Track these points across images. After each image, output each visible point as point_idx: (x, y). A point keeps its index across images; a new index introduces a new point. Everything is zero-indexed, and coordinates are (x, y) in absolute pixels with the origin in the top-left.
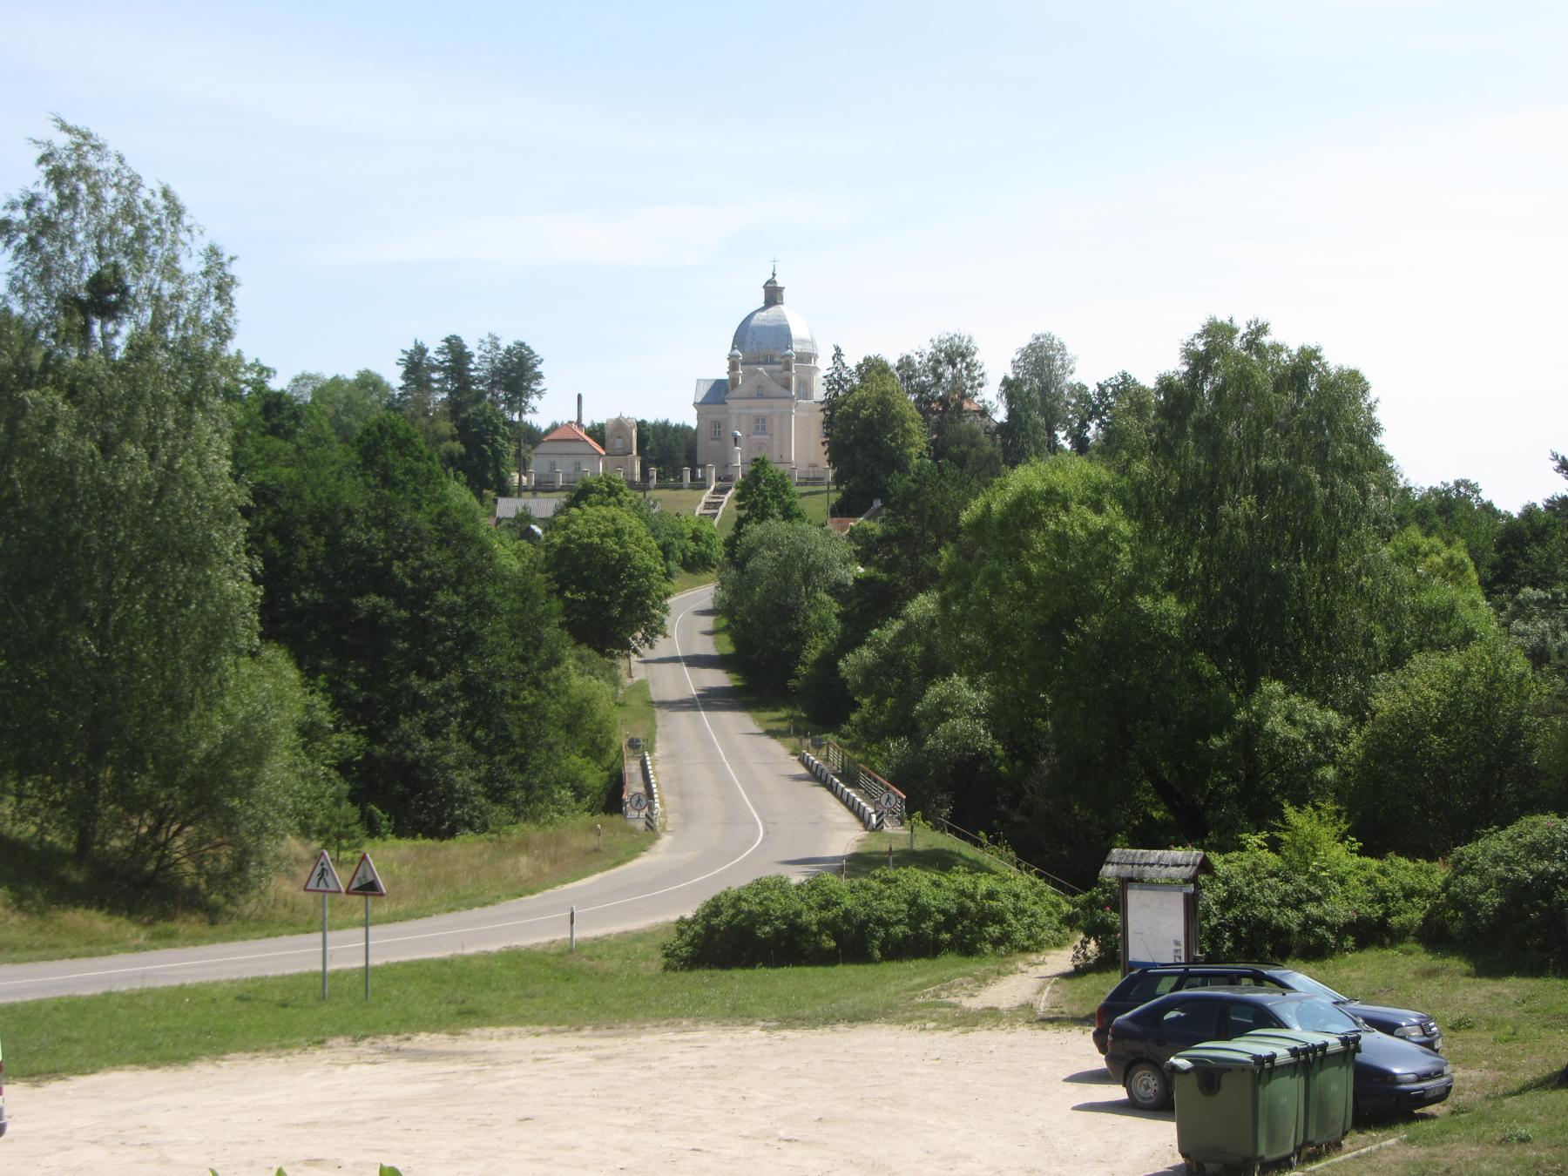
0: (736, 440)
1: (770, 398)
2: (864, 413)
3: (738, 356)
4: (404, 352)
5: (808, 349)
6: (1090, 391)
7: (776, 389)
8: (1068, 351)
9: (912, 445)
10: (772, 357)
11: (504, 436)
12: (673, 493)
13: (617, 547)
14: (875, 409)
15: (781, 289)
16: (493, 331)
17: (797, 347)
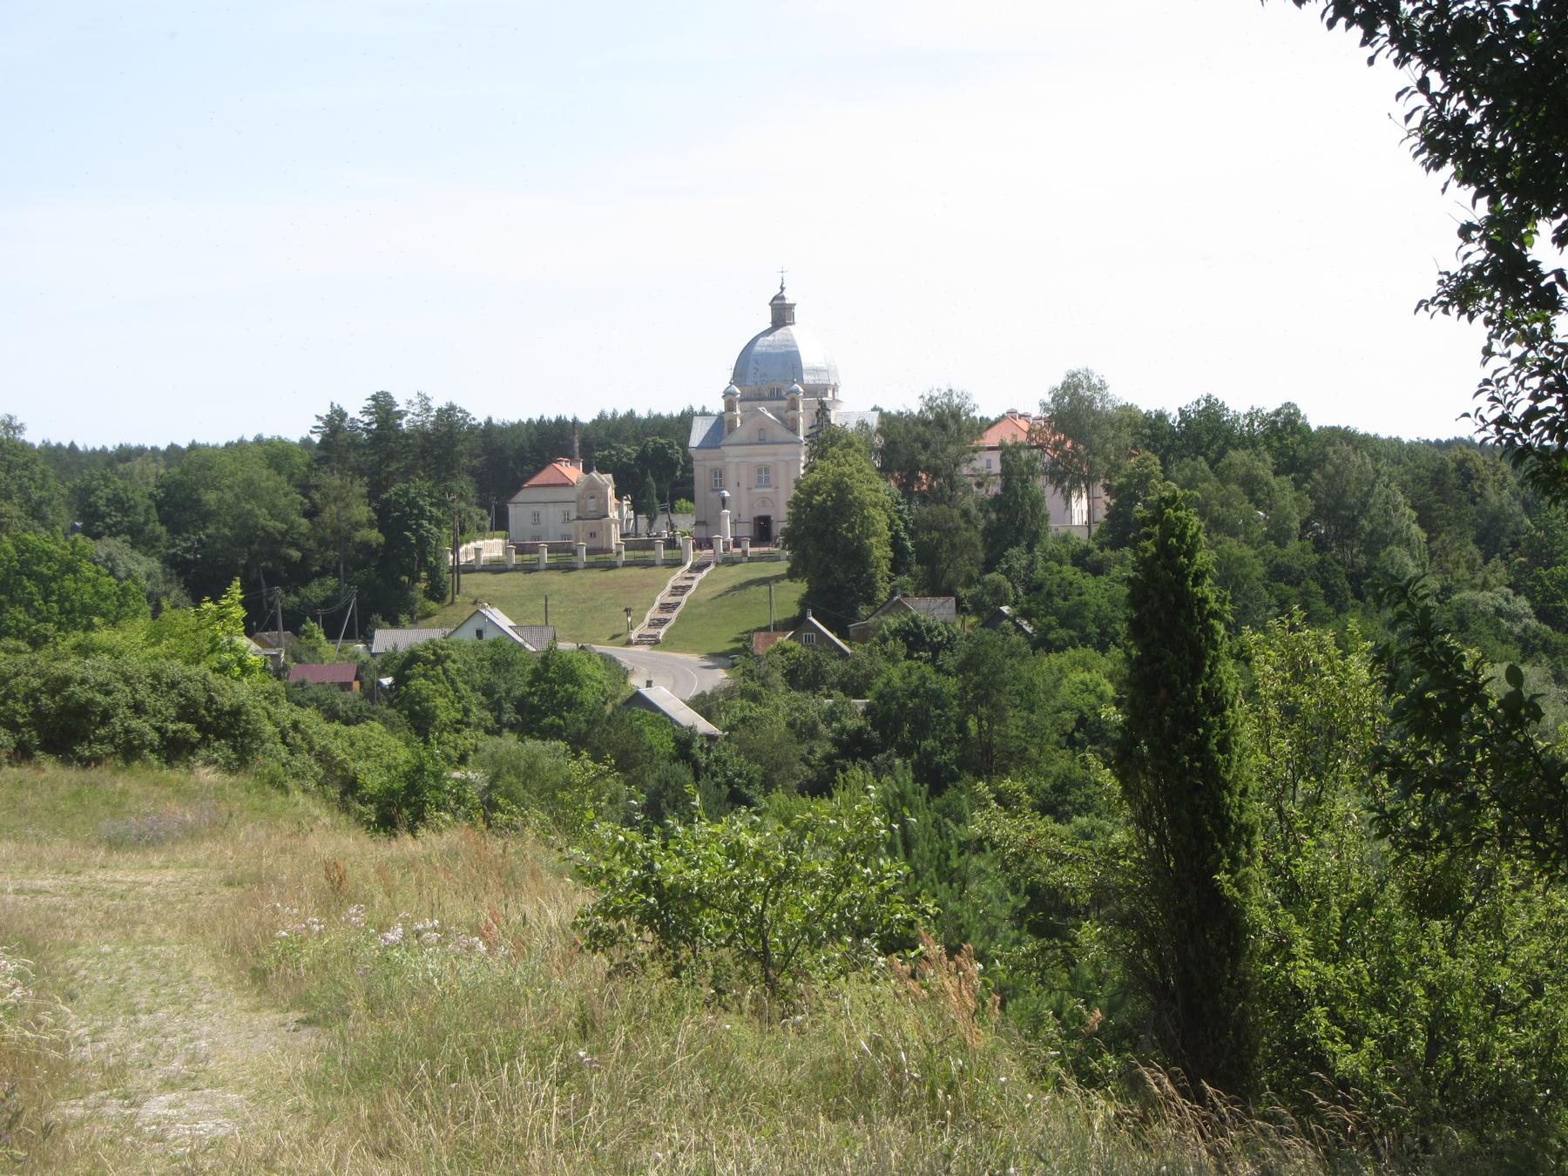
1: (774, 443)
3: (734, 394)
4: (319, 418)
5: (822, 379)
7: (783, 434)
8: (1110, 391)
9: (875, 534)
12: (643, 571)
15: (791, 306)
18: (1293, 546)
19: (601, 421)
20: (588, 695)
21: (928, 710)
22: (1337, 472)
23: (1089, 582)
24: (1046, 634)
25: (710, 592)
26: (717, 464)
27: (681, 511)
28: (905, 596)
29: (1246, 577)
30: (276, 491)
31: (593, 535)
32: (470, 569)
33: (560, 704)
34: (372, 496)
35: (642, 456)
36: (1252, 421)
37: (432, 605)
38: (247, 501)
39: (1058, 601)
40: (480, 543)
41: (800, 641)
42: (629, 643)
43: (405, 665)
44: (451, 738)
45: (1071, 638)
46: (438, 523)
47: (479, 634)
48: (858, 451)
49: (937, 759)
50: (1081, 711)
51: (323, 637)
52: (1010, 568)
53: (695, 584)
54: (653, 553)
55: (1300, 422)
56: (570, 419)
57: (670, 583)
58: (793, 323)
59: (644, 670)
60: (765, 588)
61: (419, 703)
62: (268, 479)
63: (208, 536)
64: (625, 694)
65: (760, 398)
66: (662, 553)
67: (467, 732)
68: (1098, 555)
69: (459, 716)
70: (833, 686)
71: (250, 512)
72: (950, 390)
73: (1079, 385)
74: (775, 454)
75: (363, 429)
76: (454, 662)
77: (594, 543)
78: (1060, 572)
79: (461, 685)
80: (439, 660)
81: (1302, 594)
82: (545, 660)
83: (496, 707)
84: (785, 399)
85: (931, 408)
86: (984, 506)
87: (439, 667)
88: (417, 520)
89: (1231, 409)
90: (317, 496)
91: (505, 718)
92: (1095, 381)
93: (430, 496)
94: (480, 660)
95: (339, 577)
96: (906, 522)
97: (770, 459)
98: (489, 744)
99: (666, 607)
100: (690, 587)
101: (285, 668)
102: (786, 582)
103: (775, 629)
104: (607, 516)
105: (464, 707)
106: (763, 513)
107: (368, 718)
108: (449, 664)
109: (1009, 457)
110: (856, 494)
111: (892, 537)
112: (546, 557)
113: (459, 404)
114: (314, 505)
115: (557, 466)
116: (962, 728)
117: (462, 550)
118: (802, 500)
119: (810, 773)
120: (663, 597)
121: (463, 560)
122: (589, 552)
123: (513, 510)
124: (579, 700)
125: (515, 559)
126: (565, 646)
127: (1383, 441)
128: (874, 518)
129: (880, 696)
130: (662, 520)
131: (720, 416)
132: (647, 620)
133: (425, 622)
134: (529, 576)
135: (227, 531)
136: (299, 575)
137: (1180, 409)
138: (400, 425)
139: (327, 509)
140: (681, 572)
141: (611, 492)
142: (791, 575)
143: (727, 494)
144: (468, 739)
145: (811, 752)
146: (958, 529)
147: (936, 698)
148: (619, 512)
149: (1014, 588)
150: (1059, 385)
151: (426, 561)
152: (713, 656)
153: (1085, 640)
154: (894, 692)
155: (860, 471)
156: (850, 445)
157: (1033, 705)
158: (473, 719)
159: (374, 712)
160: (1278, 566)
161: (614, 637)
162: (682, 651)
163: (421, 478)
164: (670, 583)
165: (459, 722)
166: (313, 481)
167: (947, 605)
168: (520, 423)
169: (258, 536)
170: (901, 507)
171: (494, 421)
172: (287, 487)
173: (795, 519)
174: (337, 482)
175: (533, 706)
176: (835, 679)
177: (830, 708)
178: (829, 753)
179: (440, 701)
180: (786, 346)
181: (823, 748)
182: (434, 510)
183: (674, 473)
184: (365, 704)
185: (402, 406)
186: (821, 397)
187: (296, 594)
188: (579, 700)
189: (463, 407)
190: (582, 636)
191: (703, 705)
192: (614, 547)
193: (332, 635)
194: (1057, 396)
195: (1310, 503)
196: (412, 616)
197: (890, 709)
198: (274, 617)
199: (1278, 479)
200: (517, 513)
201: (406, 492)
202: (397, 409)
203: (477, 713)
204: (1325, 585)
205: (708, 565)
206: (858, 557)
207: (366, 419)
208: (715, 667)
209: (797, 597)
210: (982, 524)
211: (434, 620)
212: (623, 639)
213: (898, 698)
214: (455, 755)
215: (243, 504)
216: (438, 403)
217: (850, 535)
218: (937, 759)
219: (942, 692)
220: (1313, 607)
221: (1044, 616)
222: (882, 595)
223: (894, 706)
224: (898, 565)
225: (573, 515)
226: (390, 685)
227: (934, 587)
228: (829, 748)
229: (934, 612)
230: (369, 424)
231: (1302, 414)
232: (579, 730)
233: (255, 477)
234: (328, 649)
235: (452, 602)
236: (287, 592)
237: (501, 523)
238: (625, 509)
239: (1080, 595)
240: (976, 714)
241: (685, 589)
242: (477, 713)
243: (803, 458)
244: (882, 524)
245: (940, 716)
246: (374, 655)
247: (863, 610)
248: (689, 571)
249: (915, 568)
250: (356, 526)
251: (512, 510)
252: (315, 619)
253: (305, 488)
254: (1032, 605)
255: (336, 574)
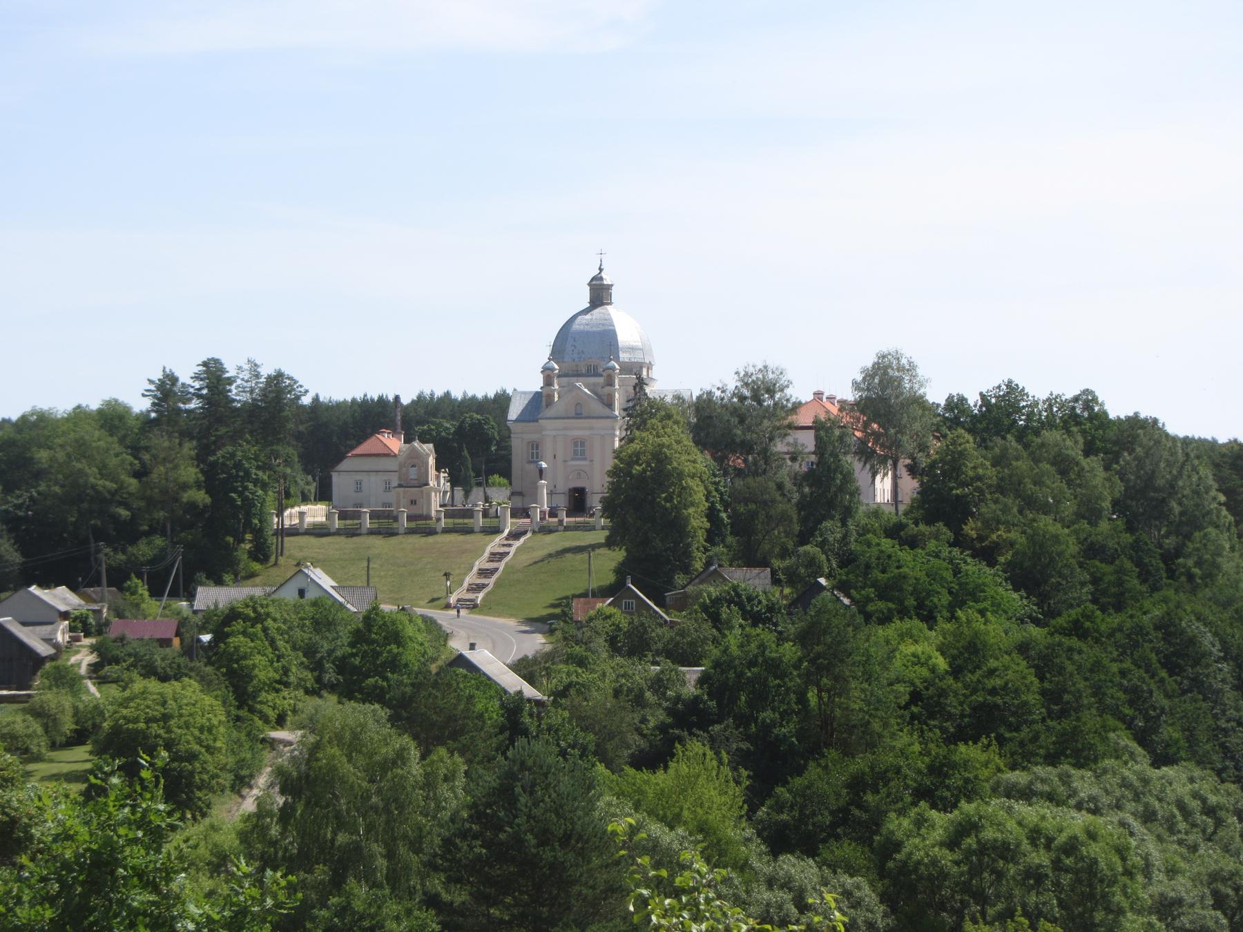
1: (589, 417)
2: (637, 469)
3: (553, 369)
4: (151, 382)
5: (637, 357)
6: (971, 402)
7: (598, 408)
9: (692, 504)
10: (595, 368)
11: (256, 482)
13: (161, 732)
14: (649, 465)
15: (609, 287)
16: (253, 357)
17: (624, 356)
18: (1104, 526)
19: (420, 401)
20: (410, 656)
21: (766, 679)
22: (1147, 453)
23: (905, 555)
24: (865, 606)
25: (526, 559)
26: (535, 437)
27: (494, 484)
28: (720, 566)
29: (1060, 554)
30: (107, 450)
31: (413, 502)
32: (294, 532)
33: (384, 665)
34: (200, 458)
35: (460, 431)
36: (1051, 406)
37: (256, 566)
38: (78, 460)
39: (877, 574)
40: (304, 508)
41: (620, 607)
42: (448, 606)
43: (223, 622)
44: (270, 698)
45: (889, 610)
46: (264, 486)
47: (302, 593)
48: (677, 422)
49: (776, 731)
50: (913, 684)
51: (146, 594)
52: (825, 542)
53: (512, 550)
54: (472, 521)
55: (1096, 409)
56: (391, 398)
57: (488, 550)
58: (610, 304)
59: (463, 633)
60: (585, 555)
61: (237, 662)
62: (99, 439)
63: (39, 493)
64: (444, 658)
65: (578, 375)
66: (480, 521)
67: (285, 693)
68: (912, 529)
69: (277, 677)
70: (658, 653)
71: (80, 471)
72: (766, 367)
73: (890, 366)
74: (591, 428)
75: (194, 394)
76: (275, 620)
77: (415, 510)
78: (878, 545)
79: (280, 643)
80: (259, 619)
81: (1117, 572)
82: (368, 620)
83: (317, 667)
84: (601, 376)
85: (746, 384)
86: (799, 480)
87: (259, 626)
88: (242, 483)
89: (1031, 394)
90: (146, 457)
91: (326, 677)
92: (904, 361)
93: (256, 459)
94: (302, 619)
95: (165, 536)
96: (721, 494)
97: (587, 433)
98: (310, 704)
99: (484, 573)
100: (508, 553)
101: (107, 623)
102: (603, 551)
103: (594, 595)
104: (427, 484)
105: (283, 667)
106: (579, 484)
107: (186, 675)
108: (269, 622)
109: (822, 433)
110: (675, 464)
111: (709, 508)
112: (367, 523)
113: (287, 371)
114: (143, 464)
115: (379, 436)
116: (802, 699)
117: (287, 513)
118: (621, 470)
119: (643, 744)
120: (481, 563)
121: (287, 523)
122: (410, 518)
123: (336, 478)
124: (403, 662)
125: (337, 524)
126: (386, 608)
127: (1167, 435)
128: (691, 489)
129: (717, 665)
130: (477, 493)
131: (537, 396)
132: (466, 585)
133: (249, 582)
134: (350, 540)
135: (57, 489)
136: (128, 534)
137: (981, 394)
138: (230, 391)
139: (155, 470)
140: (499, 539)
141: (431, 461)
142: (610, 543)
143: (544, 465)
144: (286, 699)
145: (644, 720)
146: (773, 501)
147: (774, 667)
148: (438, 482)
149: (828, 560)
150: (869, 365)
151: (251, 523)
152: (530, 621)
153: (903, 613)
154: (733, 659)
155: (678, 442)
156: (669, 417)
157: (870, 676)
158: (292, 679)
159: (191, 669)
160: (1092, 543)
161: (433, 600)
162: (494, 616)
163: (248, 442)
164: (488, 550)
165: (279, 682)
166: (143, 443)
167: (762, 575)
168: (345, 402)
169: (88, 495)
170: (717, 479)
171: (321, 399)
172: (117, 448)
173: (615, 488)
174: (166, 444)
175: (355, 667)
176: (660, 646)
177: (657, 674)
178: (663, 723)
179: (258, 659)
180: (603, 325)
181: (657, 717)
182: (260, 473)
183: (489, 448)
184: (182, 661)
185: (231, 373)
186: (638, 376)
187: (124, 552)
188: (403, 662)
189: (291, 374)
190: (402, 599)
191: (524, 668)
192: (433, 514)
193: (156, 592)
194: (869, 375)
195: (1120, 487)
196: (236, 575)
197: (727, 678)
198: (99, 573)
199: (1088, 460)
200: (341, 481)
201: (233, 455)
202: (227, 375)
203: (296, 674)
204: (1139, 563)
205: (525, 533)
206: (676, 526)
207: (197, 385)
208: (532, 632)
209: (613, 565)
210: (796, 496)
211: (258, 580)
212: (442, 602)
213: (735, 668)
214: (272, 715)
215: (74, 463)
216: (266, 370)
217: (668, 505)
218: (776, 731)
219: (782, 661)
220: (1128, 586)
221: (863, 588)
222: (698, 565)
223: (732, 675)
224: (713, 536)
225: (395, 483)
226: (210, 642)
227: (750, 558)
228: (661, 716)
229: (754, 581)
230: (199, 389)
231: (1100, 400)
232: (404, 694)
233: (87, 437)
234: (152, 606)
235: (276, 564)
236: (115, 550)
237: (324, 494)
238: (442, 481)
239: (898, 567)
240: (818, 685)
241: (503, 555)
242: (296, 674)
243: (618, 433)
244: (699, 494)
245: (779, 686)
246: (195, 612)
247: (680, 579)
248: (507, 539)
249: (730, 539)
250: (185, 487)
252: (140, 576)
253: (135, 450)
254: (850, 576)
255: (163, 533)
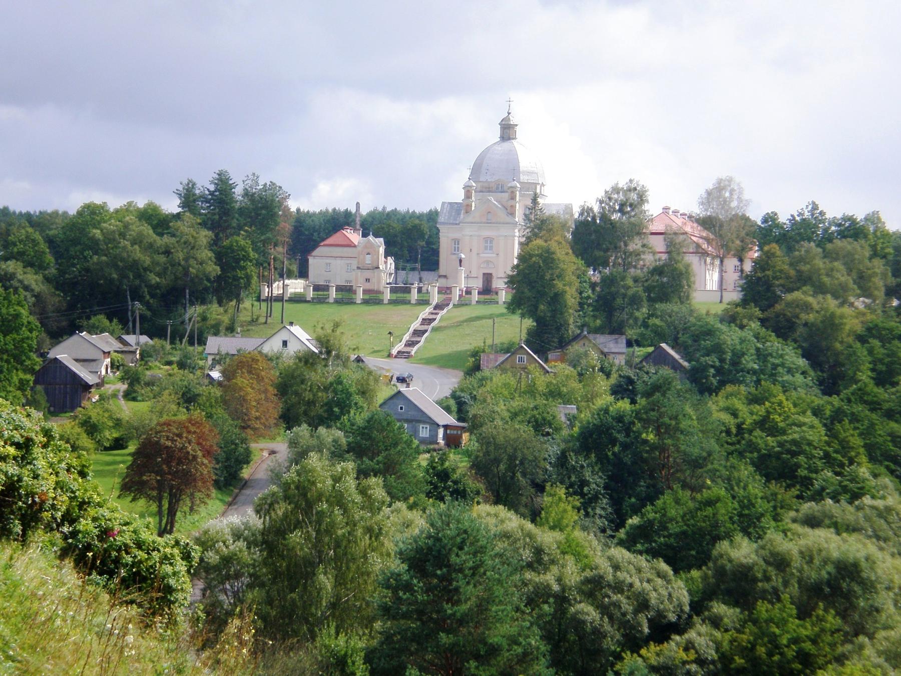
0: (461, 261)
7: (502, 216)
47: (285, 343)
77: (368, 286)
251: (311, 261)
